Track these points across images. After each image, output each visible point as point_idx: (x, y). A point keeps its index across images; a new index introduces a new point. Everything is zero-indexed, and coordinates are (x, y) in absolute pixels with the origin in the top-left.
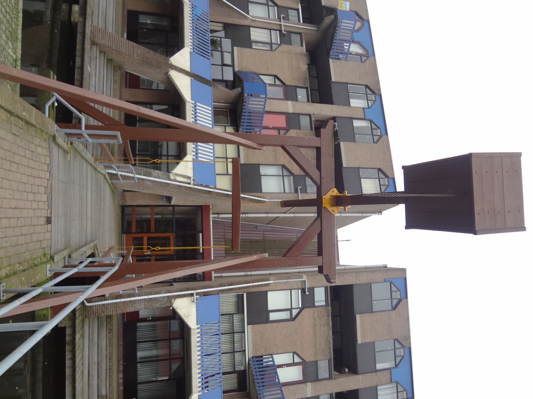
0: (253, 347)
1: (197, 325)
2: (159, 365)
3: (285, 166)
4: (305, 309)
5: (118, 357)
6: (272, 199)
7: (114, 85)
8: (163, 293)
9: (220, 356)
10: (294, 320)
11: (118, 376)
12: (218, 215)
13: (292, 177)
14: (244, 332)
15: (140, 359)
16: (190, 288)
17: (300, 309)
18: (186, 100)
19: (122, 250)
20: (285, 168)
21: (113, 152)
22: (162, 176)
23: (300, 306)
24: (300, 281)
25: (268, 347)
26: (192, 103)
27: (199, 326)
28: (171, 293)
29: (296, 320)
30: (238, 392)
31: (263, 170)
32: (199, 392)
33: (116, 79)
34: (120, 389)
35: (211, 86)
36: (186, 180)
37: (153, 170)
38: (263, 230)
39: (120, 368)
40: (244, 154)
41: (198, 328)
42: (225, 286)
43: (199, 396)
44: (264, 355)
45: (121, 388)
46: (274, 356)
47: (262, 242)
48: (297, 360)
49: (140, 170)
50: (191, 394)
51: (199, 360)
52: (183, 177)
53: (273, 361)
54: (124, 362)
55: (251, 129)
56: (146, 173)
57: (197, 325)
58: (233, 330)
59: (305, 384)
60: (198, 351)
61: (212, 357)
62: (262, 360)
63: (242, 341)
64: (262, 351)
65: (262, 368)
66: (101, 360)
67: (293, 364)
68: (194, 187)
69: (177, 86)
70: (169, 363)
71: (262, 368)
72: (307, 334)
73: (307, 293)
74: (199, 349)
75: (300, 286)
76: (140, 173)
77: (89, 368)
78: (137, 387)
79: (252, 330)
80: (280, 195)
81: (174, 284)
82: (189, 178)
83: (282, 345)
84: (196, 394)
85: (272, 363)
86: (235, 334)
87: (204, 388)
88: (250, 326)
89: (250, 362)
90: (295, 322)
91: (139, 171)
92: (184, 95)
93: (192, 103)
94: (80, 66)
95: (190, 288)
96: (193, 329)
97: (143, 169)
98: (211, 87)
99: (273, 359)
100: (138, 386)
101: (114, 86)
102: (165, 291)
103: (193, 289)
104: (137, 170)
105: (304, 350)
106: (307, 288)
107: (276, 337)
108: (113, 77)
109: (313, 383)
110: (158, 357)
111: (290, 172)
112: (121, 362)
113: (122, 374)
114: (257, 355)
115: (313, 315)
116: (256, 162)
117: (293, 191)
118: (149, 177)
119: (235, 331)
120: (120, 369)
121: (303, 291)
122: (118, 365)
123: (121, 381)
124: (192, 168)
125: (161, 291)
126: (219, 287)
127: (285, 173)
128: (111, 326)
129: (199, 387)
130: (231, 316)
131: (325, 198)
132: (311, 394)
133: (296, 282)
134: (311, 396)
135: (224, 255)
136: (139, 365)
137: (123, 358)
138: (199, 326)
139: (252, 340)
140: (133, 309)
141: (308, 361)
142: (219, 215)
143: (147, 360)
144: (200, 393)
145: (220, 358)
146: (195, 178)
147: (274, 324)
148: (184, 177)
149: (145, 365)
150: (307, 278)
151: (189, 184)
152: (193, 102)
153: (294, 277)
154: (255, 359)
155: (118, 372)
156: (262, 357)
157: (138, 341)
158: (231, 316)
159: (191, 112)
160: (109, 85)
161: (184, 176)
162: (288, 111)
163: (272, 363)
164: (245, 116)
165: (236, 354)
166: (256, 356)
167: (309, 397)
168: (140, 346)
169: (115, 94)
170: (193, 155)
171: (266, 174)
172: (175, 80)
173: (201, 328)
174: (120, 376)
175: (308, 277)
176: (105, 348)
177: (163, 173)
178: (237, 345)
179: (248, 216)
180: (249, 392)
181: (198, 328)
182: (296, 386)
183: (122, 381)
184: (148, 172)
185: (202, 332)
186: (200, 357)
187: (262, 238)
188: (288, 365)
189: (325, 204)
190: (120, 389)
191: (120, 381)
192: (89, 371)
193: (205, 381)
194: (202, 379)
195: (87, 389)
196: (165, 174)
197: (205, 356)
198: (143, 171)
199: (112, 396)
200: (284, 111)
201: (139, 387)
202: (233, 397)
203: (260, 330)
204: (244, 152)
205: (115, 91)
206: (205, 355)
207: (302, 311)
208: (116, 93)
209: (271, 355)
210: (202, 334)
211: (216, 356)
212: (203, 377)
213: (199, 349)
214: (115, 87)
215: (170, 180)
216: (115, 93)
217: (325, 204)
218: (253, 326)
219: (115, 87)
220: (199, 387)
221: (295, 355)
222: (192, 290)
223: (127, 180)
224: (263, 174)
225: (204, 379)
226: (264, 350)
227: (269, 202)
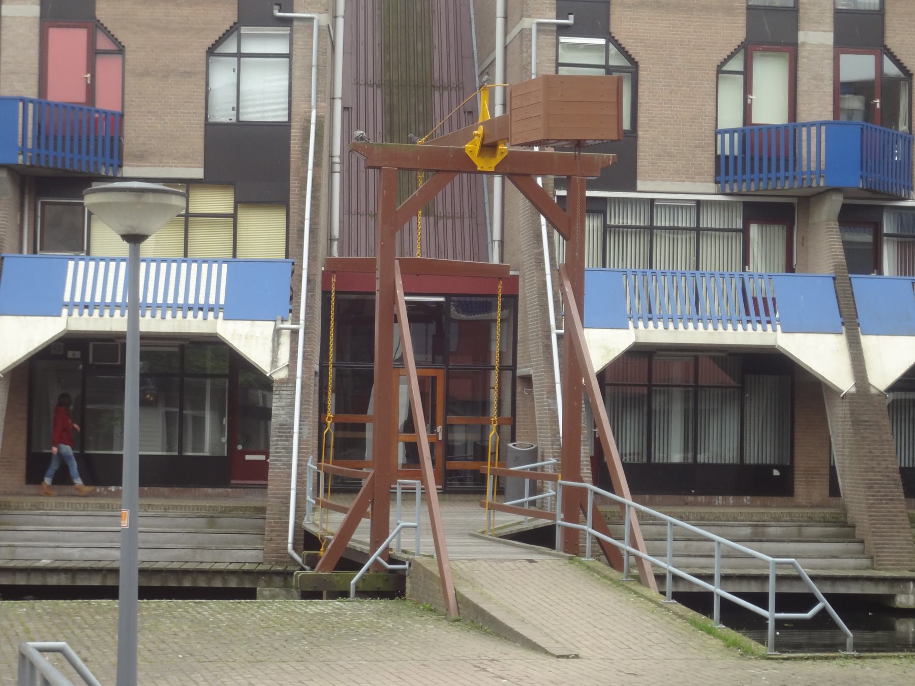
0: (692, 179)
1: (628, 328)
2: (707, 408)
3: (209, 48)
4: (612, 30)
5: (679, 505)
6: (311, 97)
7: (46, 508)
8: (555, 403)
9: (703, 275)
10: (637, 63)
11: (719, 506)
12: (335, 240)
13: (244, 30)
14: (652, 201)
15: (688, 453)
16: (544, 341)
17: (610, 44)
18: (65, 330)
19: (396, 492)
20: (215, 50)
21: (223, 509)
22: (284, 400)
23: (602, 42)
24: (537, 38)
25: (695, 139)
26: (70, 315)
27: (631, 324)
28: (554, 387)
29: (637, 59)
30: (794, 224)
31: (223, 114)
32: (774, 330)
33: (29, 504)
34: (749, 503)
35: (3, 258)
36: (285, 341)
37: (273, 420)
38: (355, 86)
39: (702, 501)
40: (176, 166)
41: (636, 327)
42: (542, 253)
43: (784, 332)
44: (714, 153)
45: (746, 499)
46: (720, 127)
47: (391, 94)
48: (736, 65)
49: (277, 448)
50: (777, 349)
51: (705, 328)
52: (278, 347)
53: (732, 132)
54: (690, 494)
55: (96, 140)
56: (281, 436)
57: (628, 328)
58: (644, 228)
59: (800, 49)
60: (686, 328)
61: (702, 293)
62: (736, 158)
63: (674, 207)
64: (705, 158)
65: (744, 159)
66: (684, 535)
67: (747, 75)
68: (302, 322)
69: (29, 353)
70: (686, 233)
71: (744, 159)
72: (678, 31)
73: (570, 21)
74: (681, 326)
75: (551, 39)
76: (284, 448)
77: (695, 556)
78: (750, 466)
79: (651, 180)
80: (297, 73)
81: (520, 371)
82: (277, 333)
83: (696, 101)
84: (778, 337)
85: (736, 135)
86: (655, 224)
87: (768, 319)
88: (640, 185)
89: (728, 191)
90: (642, 60)
91: (280, 452)
92: (50, 337)
93: (70, 315)
94: (69, 575)
95: (544, 341)
96: (637, 337)
97: (273, 441)
98: (5, 259)
99: (726, 131)
100: (748, 462)
101: (49, 508)
102: (549, 400)
103: (546, 333)
104: (278, 456)
105: (716, 43)
106: (557, 18)
107: (673, 118)
108: (24, 510)
109: (802, 23)
110: (688, 409)
111: (229, 33)
112: (690, 498)
113: (717, 497)
114: (712, 171)
115: (630, 7)
116: (200, 132)
117: (285, 31)
118: (292, 428)
119: (647, 223)
120: (704, 501)
121: (563, 30)
122: (694, 504)
123: (731, 499)
124: (250, 322)
125: (549, 410)
126: (544, 269)
127: (230, 47)
128: (614, 516)
129: (765, 330)
130: (615, 230)
131: (482, 167)
132: (826, 34)
133: (538, 48)
134: (832, 34)
135: (432, 219)
136: (701, 459)
137: (680, 494)
138: (631, 324)
139: (676, 181)
140: (587, 469)
141: (745, 35)
142: (333, 237)
143: (692, 441)
144: (779, 327)
145: (708, 276)
146: (279, 318)
147: (642, 119)
148: (279, 344)
149: (703, 435)
150: (529, 16)
151: (294, 333)
152: (65, 311)
153: (525, 55)
154: (723, 176)
155: (710, 504)
156: (718, 158)
157: (645, 460)
158: (615, 230)
159: (96, 319)
160: (58, 519)
161: (276, 344)
162: (35, 17)
163: (736, 135)
164: (63, 159)
165: (704, 224)
166: (714, 174)
167: (833, 41)
168: (658, 457)
169: (70, 505)
170: (216, 317)
171: (236, 107)
172: (15, 360)
173: (635, 317)
174: (720, 502)
175: (528, 14)
176: (659, 526)
177: (277, 396)
178: (683, 221)
179: (340, 157)
180: (799, 197)
181: (636, 327)
182: (800, 74)
183: (731, 498)
184: (280, 432)
185: (646, 318)
186: (700, 325)
187: (379, 91)
188: (748, 89)
189: (490, 168)
190: (749, 503)
191: (731, 502)
192: (701, 556)
193: (758, 299)
194: (749, 321)
195: (734, 559)
196: (277, 392)
197: (698, 314)
198: (279, 443)
199: (757, 517)
200: (36, 30)
201: (751, 458)
202: (803, 239)
203: (652, 159)
204: (171, 166)
205: (63, 506)
206: (697, 314)
207: (616, 38)
208: (68, 504)
209: (717, 132)
210: (650, 315)
211: (703, 283)
212: (745, 318)
213: (681, 326)
214: (52, 506)
215: (291, 380)
216: (68, 507)
217: (490, 168)
218: (639, 177)
219: (52, 506)
220: (765, 330)
221: (725, 68)
222: (549, 338)
223: (306, 477)
224: (234, 113)
225: (748, 318)
226: (703, 151)
227: (317, 108)
